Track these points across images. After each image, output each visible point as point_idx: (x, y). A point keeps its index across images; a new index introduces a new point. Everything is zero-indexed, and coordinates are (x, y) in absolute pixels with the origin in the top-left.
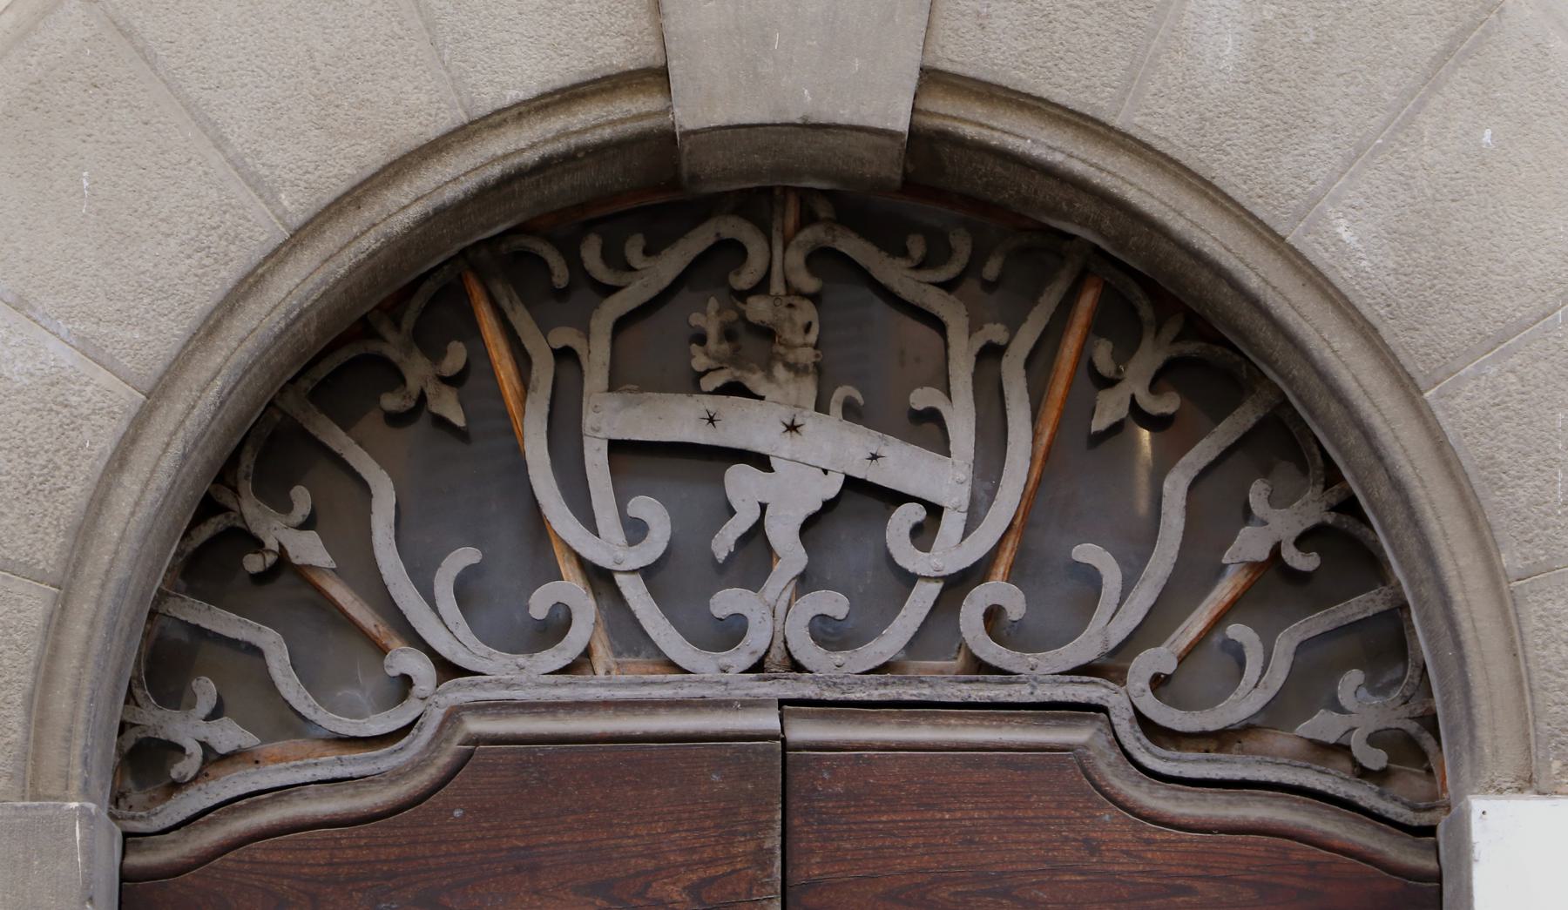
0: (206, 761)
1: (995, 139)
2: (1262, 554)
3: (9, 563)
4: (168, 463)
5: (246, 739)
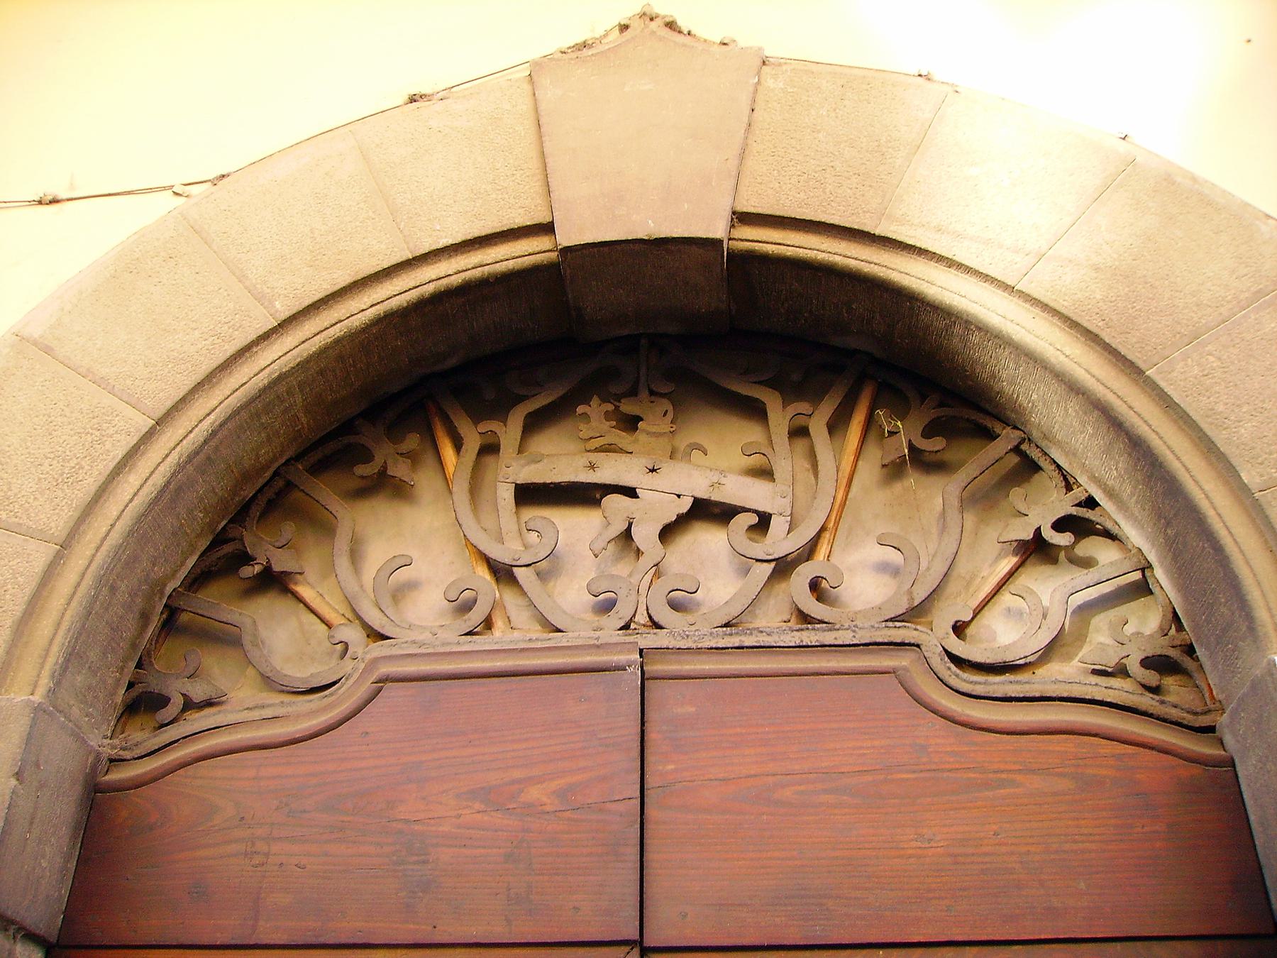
3: (31, 529)
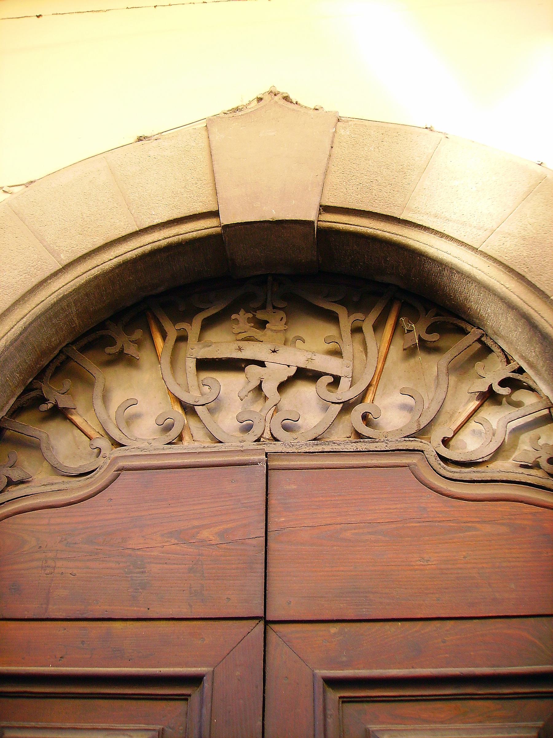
2: (485, 389)
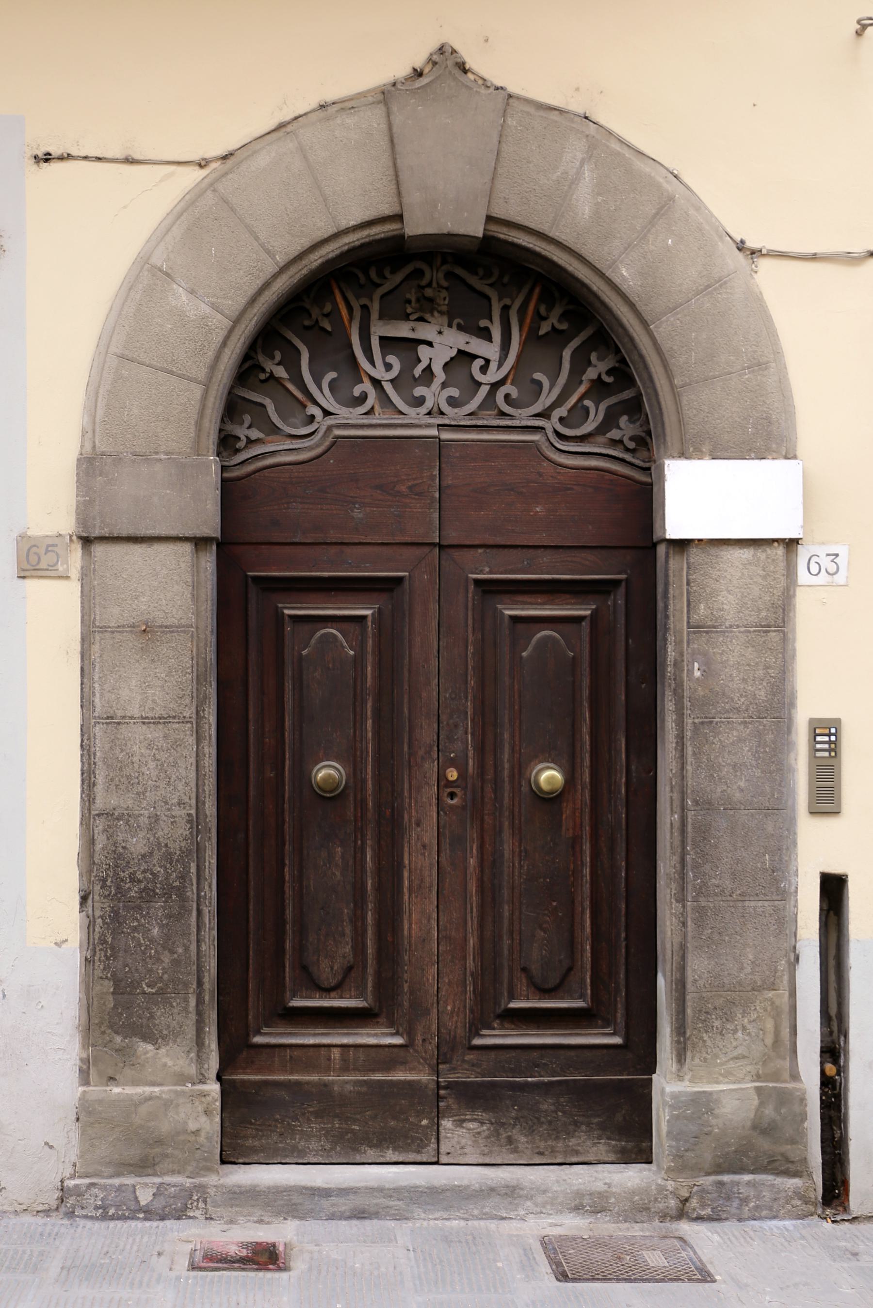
0: (247, 443)
1: (510, 239)
4: (239, 345)
5: (261, 435)
